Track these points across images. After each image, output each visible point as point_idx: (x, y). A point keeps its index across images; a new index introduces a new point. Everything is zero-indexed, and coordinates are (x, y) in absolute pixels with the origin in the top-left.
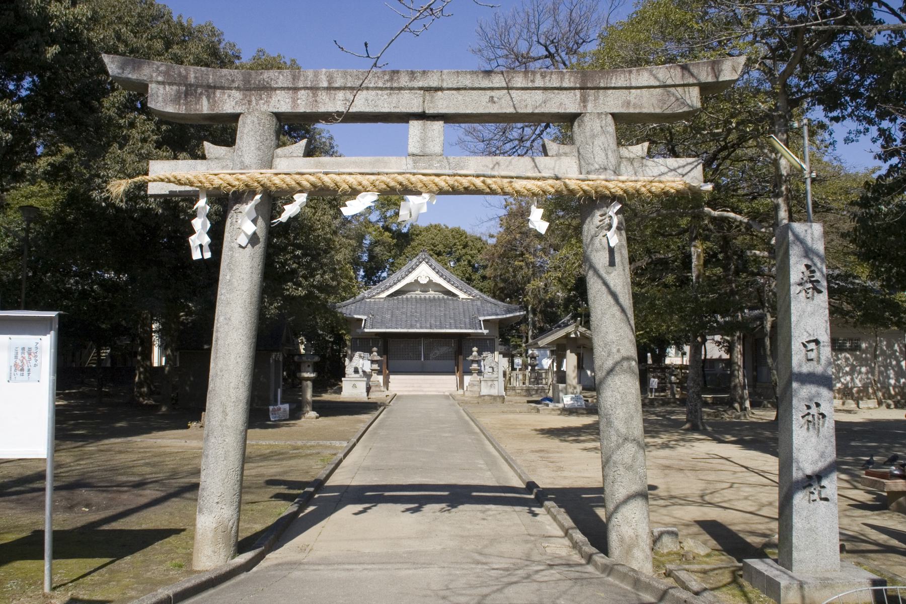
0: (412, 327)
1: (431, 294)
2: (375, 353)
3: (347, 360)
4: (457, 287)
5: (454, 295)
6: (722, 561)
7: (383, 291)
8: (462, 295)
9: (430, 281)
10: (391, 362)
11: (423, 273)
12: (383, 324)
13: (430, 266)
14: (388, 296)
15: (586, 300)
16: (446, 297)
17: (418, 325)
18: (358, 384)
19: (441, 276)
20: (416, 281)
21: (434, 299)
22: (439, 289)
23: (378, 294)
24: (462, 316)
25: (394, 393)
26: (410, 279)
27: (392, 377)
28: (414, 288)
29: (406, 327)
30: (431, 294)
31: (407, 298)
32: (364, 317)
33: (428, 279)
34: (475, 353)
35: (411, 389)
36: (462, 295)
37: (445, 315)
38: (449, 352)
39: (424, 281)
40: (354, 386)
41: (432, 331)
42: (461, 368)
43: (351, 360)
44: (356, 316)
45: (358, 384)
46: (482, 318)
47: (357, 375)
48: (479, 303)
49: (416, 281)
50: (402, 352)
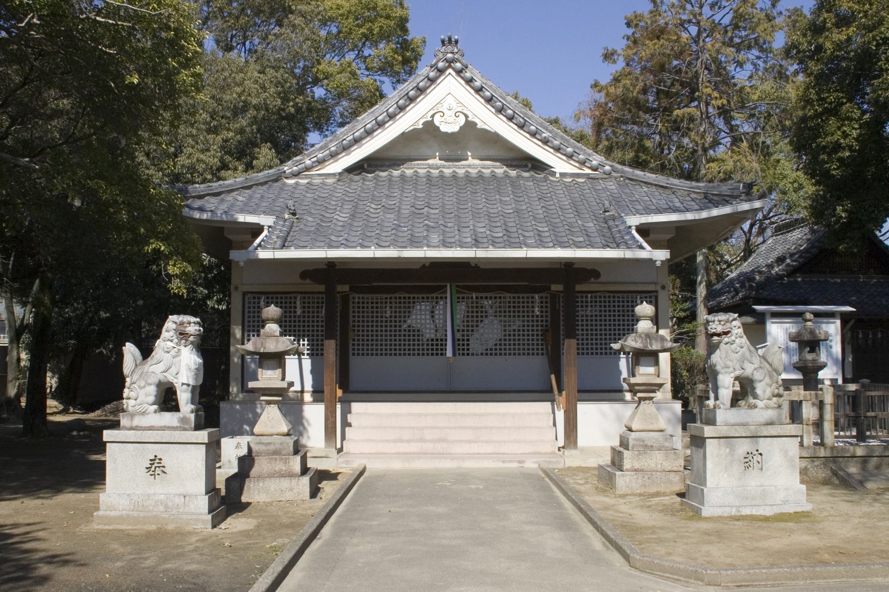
0: (414, 242)
1: (472, 165)
2: (273, 328)
3: (130, 350)
4: (545, 142)
5: (537, 165)
6: (201, 209)
7: (333, 155)
8: (560, 165)
9: (469, 125)
10: (357, 363)
11: (450, 100)
12: (320, 237)
13: (469, 81)
14: (350, 170)
15: (220, 448)
16: (513, 173)
17: (435, 238)
18: (171, 457)
19: (500, 111)
20: (430, 128)
21: (481, 176)
22: (493, 152)
23: (321, 162)
24: (571, 216)
25: (357, 464)
26: (411, 119)
27: (356, 407)
28: (424, 150)
29: (394, 244)
30: (472, 165)
31: (403, 177)
32: (266, 221)
33: (462, 121)
34: (644, 326)
35: (414, 448)
36: (560, 165)
37: (517, 211)
38: (544, 325)
39: (450, 125)
40: (155, 466)
41: (481, 254)
42: (571, 378)
43: (146, 351)
44: (241, 218)
45: (171, 457)
46: (634, 221)
47: (169, 418)
48: (612, 186)
49: (430, 128)
50: (373, 324)
